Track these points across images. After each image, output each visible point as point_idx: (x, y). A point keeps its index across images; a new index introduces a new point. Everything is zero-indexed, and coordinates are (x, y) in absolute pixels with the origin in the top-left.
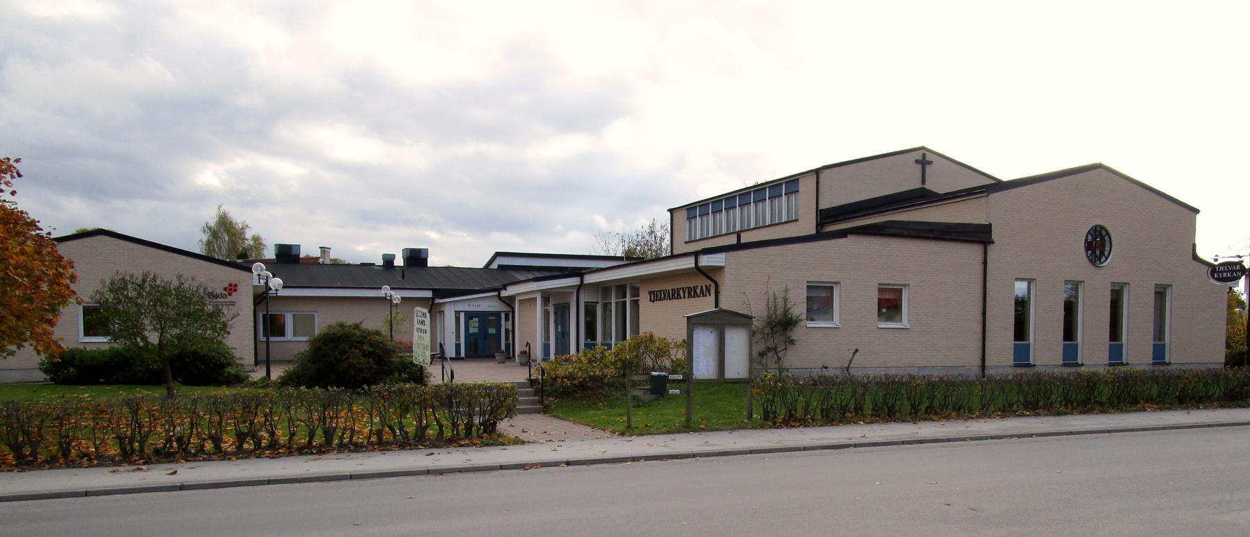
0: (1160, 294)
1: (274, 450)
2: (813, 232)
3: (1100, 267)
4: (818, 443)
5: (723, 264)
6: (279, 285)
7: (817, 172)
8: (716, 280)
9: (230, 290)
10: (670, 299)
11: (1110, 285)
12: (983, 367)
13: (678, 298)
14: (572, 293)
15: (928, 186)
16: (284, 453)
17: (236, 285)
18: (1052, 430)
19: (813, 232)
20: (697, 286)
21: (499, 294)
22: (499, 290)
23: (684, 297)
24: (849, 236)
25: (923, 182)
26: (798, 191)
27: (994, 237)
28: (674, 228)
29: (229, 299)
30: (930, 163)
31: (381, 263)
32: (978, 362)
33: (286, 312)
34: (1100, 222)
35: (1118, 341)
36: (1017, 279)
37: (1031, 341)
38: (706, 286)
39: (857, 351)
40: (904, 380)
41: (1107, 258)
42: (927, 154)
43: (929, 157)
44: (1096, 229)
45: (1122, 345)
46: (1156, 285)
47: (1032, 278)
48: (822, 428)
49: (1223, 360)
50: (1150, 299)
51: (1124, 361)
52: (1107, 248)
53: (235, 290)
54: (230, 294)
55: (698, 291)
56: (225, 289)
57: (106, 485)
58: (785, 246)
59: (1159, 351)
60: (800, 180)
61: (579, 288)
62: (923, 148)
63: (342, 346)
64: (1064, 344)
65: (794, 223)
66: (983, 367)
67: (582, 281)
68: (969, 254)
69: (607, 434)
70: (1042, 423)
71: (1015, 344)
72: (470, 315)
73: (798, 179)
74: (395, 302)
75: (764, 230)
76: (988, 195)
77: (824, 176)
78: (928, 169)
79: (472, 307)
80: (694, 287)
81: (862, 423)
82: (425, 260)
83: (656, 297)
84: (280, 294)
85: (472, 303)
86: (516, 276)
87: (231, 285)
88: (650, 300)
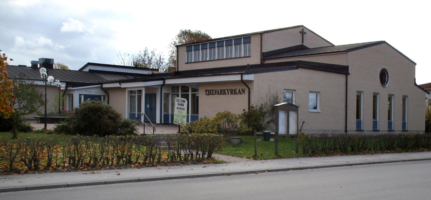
0: (404, 99)
1: (160, 163)
2: (259, 63)
3: (384, 87)
4: (367, 162)
5: (253, 79)
6: (52, 80)
7: (261, 34)
8: (249, 86)
10: (219, 94)
11: (402, 96)
13: (224, 94)
14: (158, 88)
15: (305, 44)
19: (259, 63)
20: (237, 89)
21: (102, 86)
22: (102, 84)
23: (228, 94)
24: (299, 68)
25: (303, 42)
26: (250, 42)
27: (350, 72)
28: (179, 55)
31: (30, 65)
32: (344, 129)
34: (384, 67)
35: (359, 119)
37: (361, 119)
38: (242, 89)
39: (304, 122)
40: (329, 136)
41: (387, 83)
42: (305, 29)
43: (305, 31)
44: (383, 70)
45: (392, 122)
46: (403, 96)
47: (362, 91)
50: (401, 102)
51: (393, 129)
52: (387, 79)
55: (237, 91)
57: (211, 177)
58: (283, 71)
60: (251, 37)
61: (162, 86)
62: (302, 26)
63: (99, 113)
65: (249, 58)
67: (164, 82)
68: (340, 78)
69: (245, 159)
70: (400, 156)
72: (86, 97)
73: (250, 37)
74: (62, 89)
75: (232, 60)
76: (347, 53)
77: (265, 36)
78: (305, 36)
79: (87, 92)
80: (235, 89)
81: (338, 155)
82: (52, 65)
83: (209, 93)
84: (52, 84)
85: (87, 90)
86: (100, 76)
88: (206, 94)
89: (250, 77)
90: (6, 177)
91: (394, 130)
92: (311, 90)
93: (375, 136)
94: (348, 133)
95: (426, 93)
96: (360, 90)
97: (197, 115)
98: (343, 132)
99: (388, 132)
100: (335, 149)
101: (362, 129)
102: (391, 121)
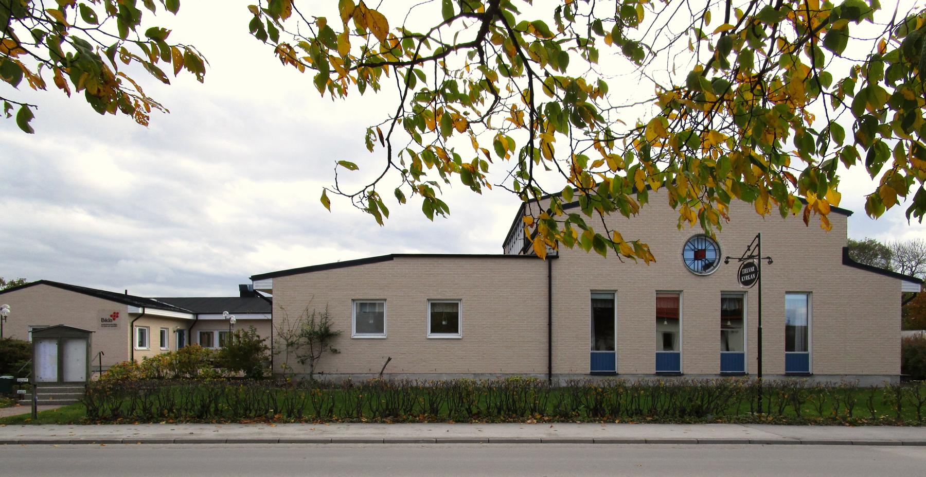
9: (114, 316)
12: (550, 374)
17: (118, 313)
18: (302, 437)
24: (394, 258)
29: (114, 322)
31: (237, 294)
32: (546, 370)
33: (214, 330)
35: (672, 349)
36: (788, 293)
39: (389, 359)
41: (715, 267)
48: (679, 425)
49: (898, 371)
53: (117, 317)
54: (114, 319)
56: (111, 316)
64: (786, 354)
66: (550, 374)
71: (786, 354)
87: (114, 313)
89: (264, 284)
90: (70, 437)
91: (812, 374)
92: (429, 298)
93: (343, 383)
94: (764, 379)
95: (903, 281)
96: (612, 289)
97: (806, 352)
98: (543, 377)
99: (785, 379)
100: (683, 412)
101: (810, 371)
102: (675, 352)
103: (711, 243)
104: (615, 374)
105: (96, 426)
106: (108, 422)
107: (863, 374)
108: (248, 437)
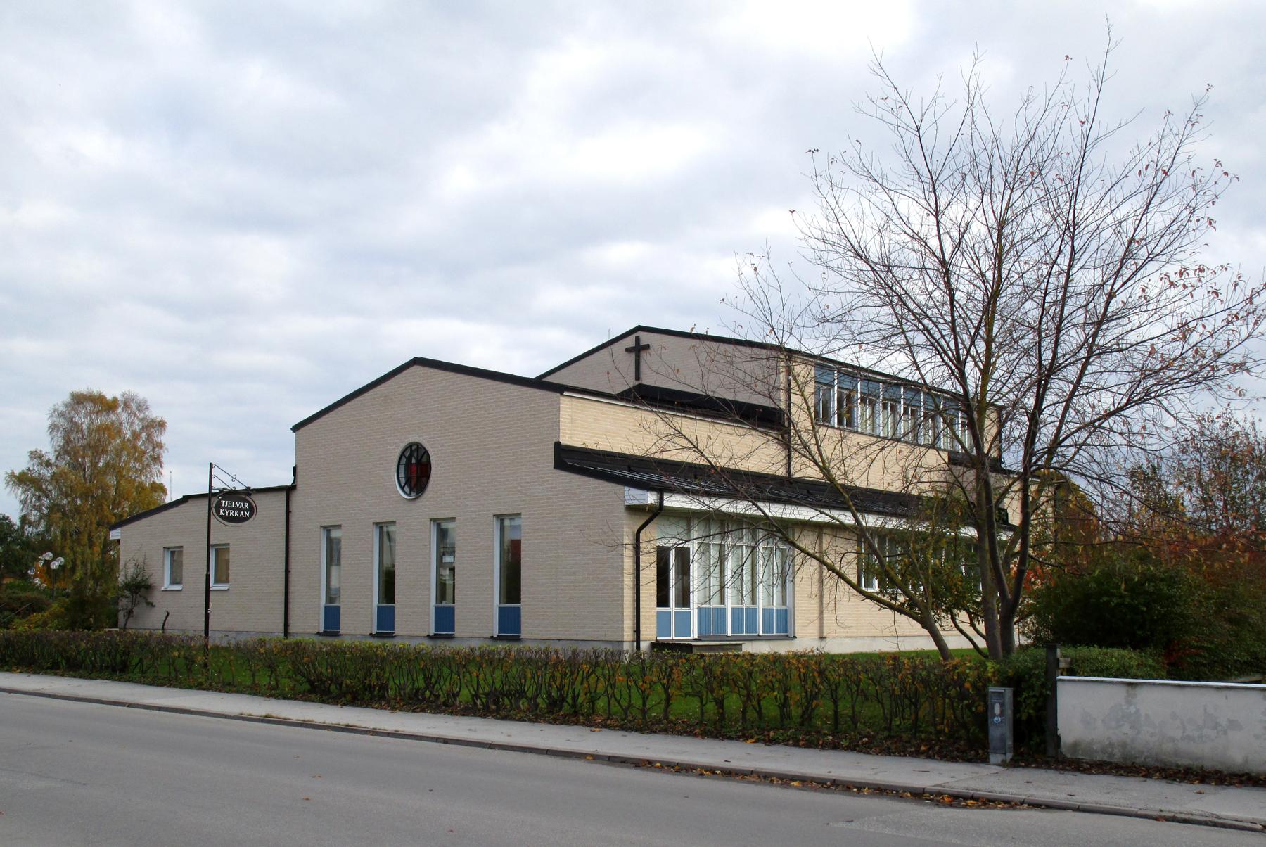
16: (973, 805)
25: (638, 377)
30: (647, 347)
34: (414, 438)
59: (510, 622)
95: (627, 488)
99: (317, 639)
103: (939, 351)
104: (517, 639)
105: (667, 736)
106: (6, 667)
107: (578, 638)
108: (964, 785)
